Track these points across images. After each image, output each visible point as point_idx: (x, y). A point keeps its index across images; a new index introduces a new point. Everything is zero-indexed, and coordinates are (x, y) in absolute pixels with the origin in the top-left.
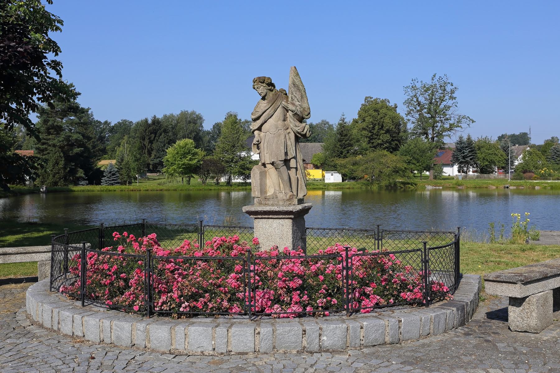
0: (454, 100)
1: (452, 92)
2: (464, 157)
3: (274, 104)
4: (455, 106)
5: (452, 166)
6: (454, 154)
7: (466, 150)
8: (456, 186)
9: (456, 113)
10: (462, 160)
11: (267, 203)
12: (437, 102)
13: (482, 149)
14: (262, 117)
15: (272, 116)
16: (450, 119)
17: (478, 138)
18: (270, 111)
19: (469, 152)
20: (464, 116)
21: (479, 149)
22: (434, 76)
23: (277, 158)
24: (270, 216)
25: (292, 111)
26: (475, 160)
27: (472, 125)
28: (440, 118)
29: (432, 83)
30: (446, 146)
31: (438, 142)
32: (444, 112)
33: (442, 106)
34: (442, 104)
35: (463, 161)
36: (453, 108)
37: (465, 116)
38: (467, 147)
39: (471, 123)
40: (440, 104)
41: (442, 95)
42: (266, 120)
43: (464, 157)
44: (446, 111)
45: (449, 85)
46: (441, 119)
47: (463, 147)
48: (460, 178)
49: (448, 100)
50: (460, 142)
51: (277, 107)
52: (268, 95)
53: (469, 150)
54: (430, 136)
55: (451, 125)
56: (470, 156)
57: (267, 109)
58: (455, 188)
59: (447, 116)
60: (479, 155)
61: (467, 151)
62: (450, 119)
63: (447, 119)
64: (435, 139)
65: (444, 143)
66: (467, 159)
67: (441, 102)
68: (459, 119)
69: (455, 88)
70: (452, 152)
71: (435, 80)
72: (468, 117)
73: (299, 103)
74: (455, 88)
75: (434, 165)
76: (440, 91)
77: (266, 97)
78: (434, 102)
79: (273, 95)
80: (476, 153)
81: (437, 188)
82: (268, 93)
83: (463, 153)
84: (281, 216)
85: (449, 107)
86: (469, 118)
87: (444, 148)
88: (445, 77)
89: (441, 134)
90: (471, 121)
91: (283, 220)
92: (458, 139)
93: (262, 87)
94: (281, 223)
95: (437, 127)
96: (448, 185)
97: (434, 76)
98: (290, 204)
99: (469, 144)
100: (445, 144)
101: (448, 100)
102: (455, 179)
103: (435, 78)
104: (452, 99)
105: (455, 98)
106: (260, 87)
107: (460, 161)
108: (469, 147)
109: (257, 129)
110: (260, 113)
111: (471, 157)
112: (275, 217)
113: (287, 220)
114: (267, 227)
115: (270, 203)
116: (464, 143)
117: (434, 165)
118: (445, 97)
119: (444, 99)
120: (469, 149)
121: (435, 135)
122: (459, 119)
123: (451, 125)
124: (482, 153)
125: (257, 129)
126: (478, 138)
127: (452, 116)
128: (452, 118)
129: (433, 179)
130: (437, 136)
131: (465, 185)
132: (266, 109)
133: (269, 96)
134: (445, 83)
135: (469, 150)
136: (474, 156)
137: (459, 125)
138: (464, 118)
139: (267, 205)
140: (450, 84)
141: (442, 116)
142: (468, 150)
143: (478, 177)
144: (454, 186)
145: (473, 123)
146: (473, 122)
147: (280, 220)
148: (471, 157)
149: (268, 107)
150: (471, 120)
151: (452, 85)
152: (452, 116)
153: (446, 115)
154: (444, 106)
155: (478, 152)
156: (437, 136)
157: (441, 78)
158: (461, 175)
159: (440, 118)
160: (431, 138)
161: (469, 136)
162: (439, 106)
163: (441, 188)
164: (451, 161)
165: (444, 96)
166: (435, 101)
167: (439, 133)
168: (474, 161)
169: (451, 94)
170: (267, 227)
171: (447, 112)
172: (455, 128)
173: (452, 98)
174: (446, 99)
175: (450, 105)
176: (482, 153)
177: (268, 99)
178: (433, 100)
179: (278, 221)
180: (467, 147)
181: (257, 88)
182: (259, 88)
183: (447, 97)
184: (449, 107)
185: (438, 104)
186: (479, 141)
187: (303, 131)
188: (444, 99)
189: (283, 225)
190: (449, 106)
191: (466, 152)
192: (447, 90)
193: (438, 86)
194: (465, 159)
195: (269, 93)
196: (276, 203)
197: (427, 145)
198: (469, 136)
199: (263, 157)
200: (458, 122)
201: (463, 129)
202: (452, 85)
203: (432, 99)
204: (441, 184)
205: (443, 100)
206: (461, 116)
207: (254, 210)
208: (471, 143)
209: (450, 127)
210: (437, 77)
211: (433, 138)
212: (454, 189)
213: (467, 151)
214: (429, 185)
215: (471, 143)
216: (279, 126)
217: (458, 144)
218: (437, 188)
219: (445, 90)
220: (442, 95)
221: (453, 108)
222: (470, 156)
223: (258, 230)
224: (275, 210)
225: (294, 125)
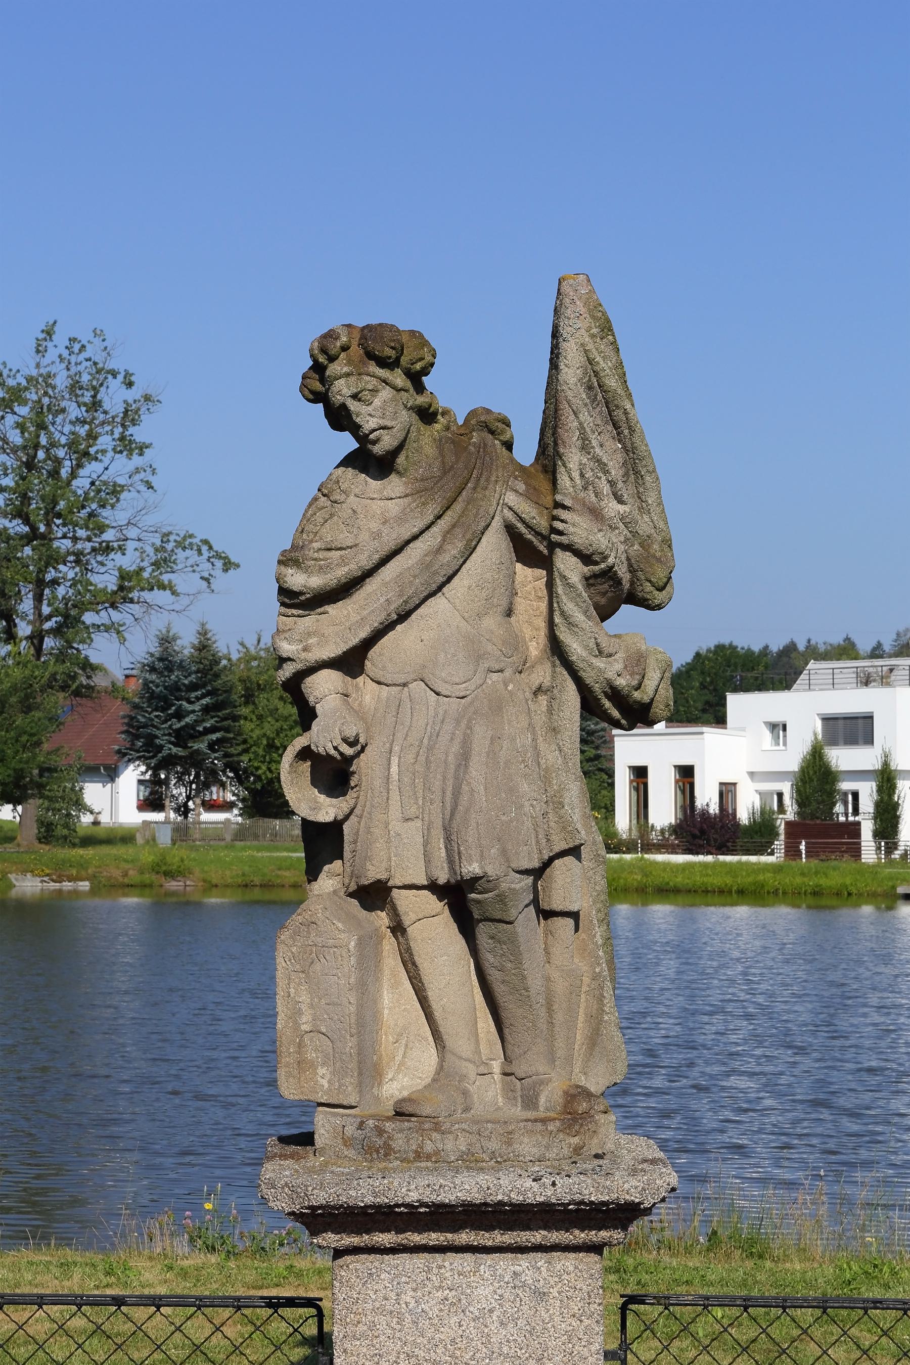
0: (135, 457)
1: (130, 416)
2: (182, 737)
3: (458, 507)
4: (143, 488)
5: (111, 774)
6: (132, 718)
7: (190, 702)
8: (154, 877)
9: (149, 520)
10: (175, 750)
11: (429, 1147)
12: (58, 462)
13: (262, 699)
14: (371, 586)
15: (449, 579)
16: (122, 549)
17: (242, 644)
18: (439, 550)
19: (206, 710)
20: (184, 538)
21: (249, 698)
22: (49, 333)
23: (504, 852)
24: (464, 1237)
25: (586, 558)
26: (232, 750)
27: (221, 580)
28: (75, 539)
29: (38, 366)
30: (99, 681)
31: (61, 657)
32: (92, 515)
33: (81, 484)
34: (82, 472)
35: (176, 756)
36: (134, 494)
37: (191, 536)
38: (193, 687)
39: (218, 572)
40: (73, 475)
41: (83, 431)
42: (410, 606)
43: (182, 737)
44: (103, 506)
45: (115, 384)
46: (79, 546)
47: (175, 688)
48: (165, 838)
49: (110, 454)
50: (161, 659)
51: (483, 524)
52: (411, 445)
53: (204, 701)
54: (24, 629)
55: (124, 576)
56: (207, 731)
57: (415, 538)
58: (151, 886)
59: (109, 535)
60: (247, 726)
61: (197, 707)
62: (122, 549)
63: (107, 549)
64: (49, 643)
65: (87, 666)
66: (196, 746)
67: (79, 466)
68: (163, 549)
69: (147, 398)
70: (125, 710)
71: (52, 355)
72: (206, 542)
73: (621, 508)
74: (147, 398)
75: (43, 770)
76: (74, 411)
77: (401, 460)
78: (45, 461)
79: (440, 443)
80: (235, 718)
81: (67, 885)
82: (413, 435)
83: (179, 715)
84: (538, 1237)
85: (116, 490)
86: (211, 548)
87: (88, 687)
88: (97, 341)
89: (78, 620)
90: (219, 564)
91: (540, 1259)
92: (154, 647)
93: (386, 393)
94: (528, 1277)
95: (55, 582)
96: (117, 873)
97: (49, 333)
98: (577, 1150)
99: (204, 672)
100: (94, 668)
101: (110, 454)
102: (140, 840)
103: (50, 344)
104: (131, 452)
105: (142, 449)
106: (375, 391)
107: (165, 752)
108: (204, 686)
109: (334, 664)
110: (365, 560)
111: (214, 737)
112: (498, 1237)
113: (568, 1262)
114: (431, 1307)
115: (449, 1146)
116: (181, 666)
117: (43, 770)
118: (96, 438)
119: (92, 450)
120: (203, 696)
121: (47, 625)
122: (163, 549)
123: (124, 576)
124: (260, 718)
125: (334, 664)
126: (242, 644)
127: (132, 533)
128: (130, 545)
129: (36, 843)
130: (57, 632)
131: (197, 870)
132: (407, 536)
133: (419, 450)
134: (99, 372)
135: (204, 701)
136: (227, 730)
137: (165, 578)
138: (184, 549)
139: (428, 1157)
140: (120, 378)
141: (82, 533)
142: (198, 699)
143: (241, 834)
144: (147, 877)
145: (226, 570)
146: (228, 565)
147: (523, 1262)
148: (214, 737)
149: (420, 524)
150: (218, 556)
151: (130, 385)
152: (132, 533)
153: (102, 529)
154: (93, 483)
155: (245, 711)
156: (57, 632)
157: (77, 347)
158: (167, 821)
159: (75, 539)
160: (30, 638)
161: (203, 633)
162: (69, 483)
163: (85, 885)
164: (119, 752)
165: (92, 436)
166: (48, 457)
167: (66, 616)
168: (226, 755)
169: (123, 425)
170: (431, 1307)
171: (105, 512)
172: (146, 595)
173: (127, 446)
174: (104, 452)
175: (121, 481)
176: (260, 718)
177: (413, 473)
178: (41, 455)
179: (505, 1264)
180: (193, 687)
181: (355, 397)
182: (366, 395)
183: (105, 441)
184: (116, 490)
185: (64, 472)
186: (248, 658)
187: (638, 688)
188: (92, 450)
189: (541, 1295)
190: (115, 485)
191: (193, 708)
192: (106, 406)
193: (61, 381)
194: (185, 747)
195: (419, 430)
196: (494, 1145)
197: (17, 674)
198: (203, 633)
199: (380, 845)
200: (156, 564)
201: (184, 601)
202: (130, 385)
203: (37, 446)
204: (82, 865)
205: (86, 454)
206: (172, 538)
207: (369, 1200)
208: (215, 669)
209: (121, 588)
210: (60, 339)
211: (37, 638)
212: (147, 891)
213: (197, 707)
214: (24, 872)
215: (215, 669)
216: (490, 647)
217: (153, 669)
218: (67, 885)
219: (95, 405)
220: (83, 431)
221: (134, 494)
222: (207, 731)
223: (362, 1328)
224: (516, 1198)
225: (592, 644)
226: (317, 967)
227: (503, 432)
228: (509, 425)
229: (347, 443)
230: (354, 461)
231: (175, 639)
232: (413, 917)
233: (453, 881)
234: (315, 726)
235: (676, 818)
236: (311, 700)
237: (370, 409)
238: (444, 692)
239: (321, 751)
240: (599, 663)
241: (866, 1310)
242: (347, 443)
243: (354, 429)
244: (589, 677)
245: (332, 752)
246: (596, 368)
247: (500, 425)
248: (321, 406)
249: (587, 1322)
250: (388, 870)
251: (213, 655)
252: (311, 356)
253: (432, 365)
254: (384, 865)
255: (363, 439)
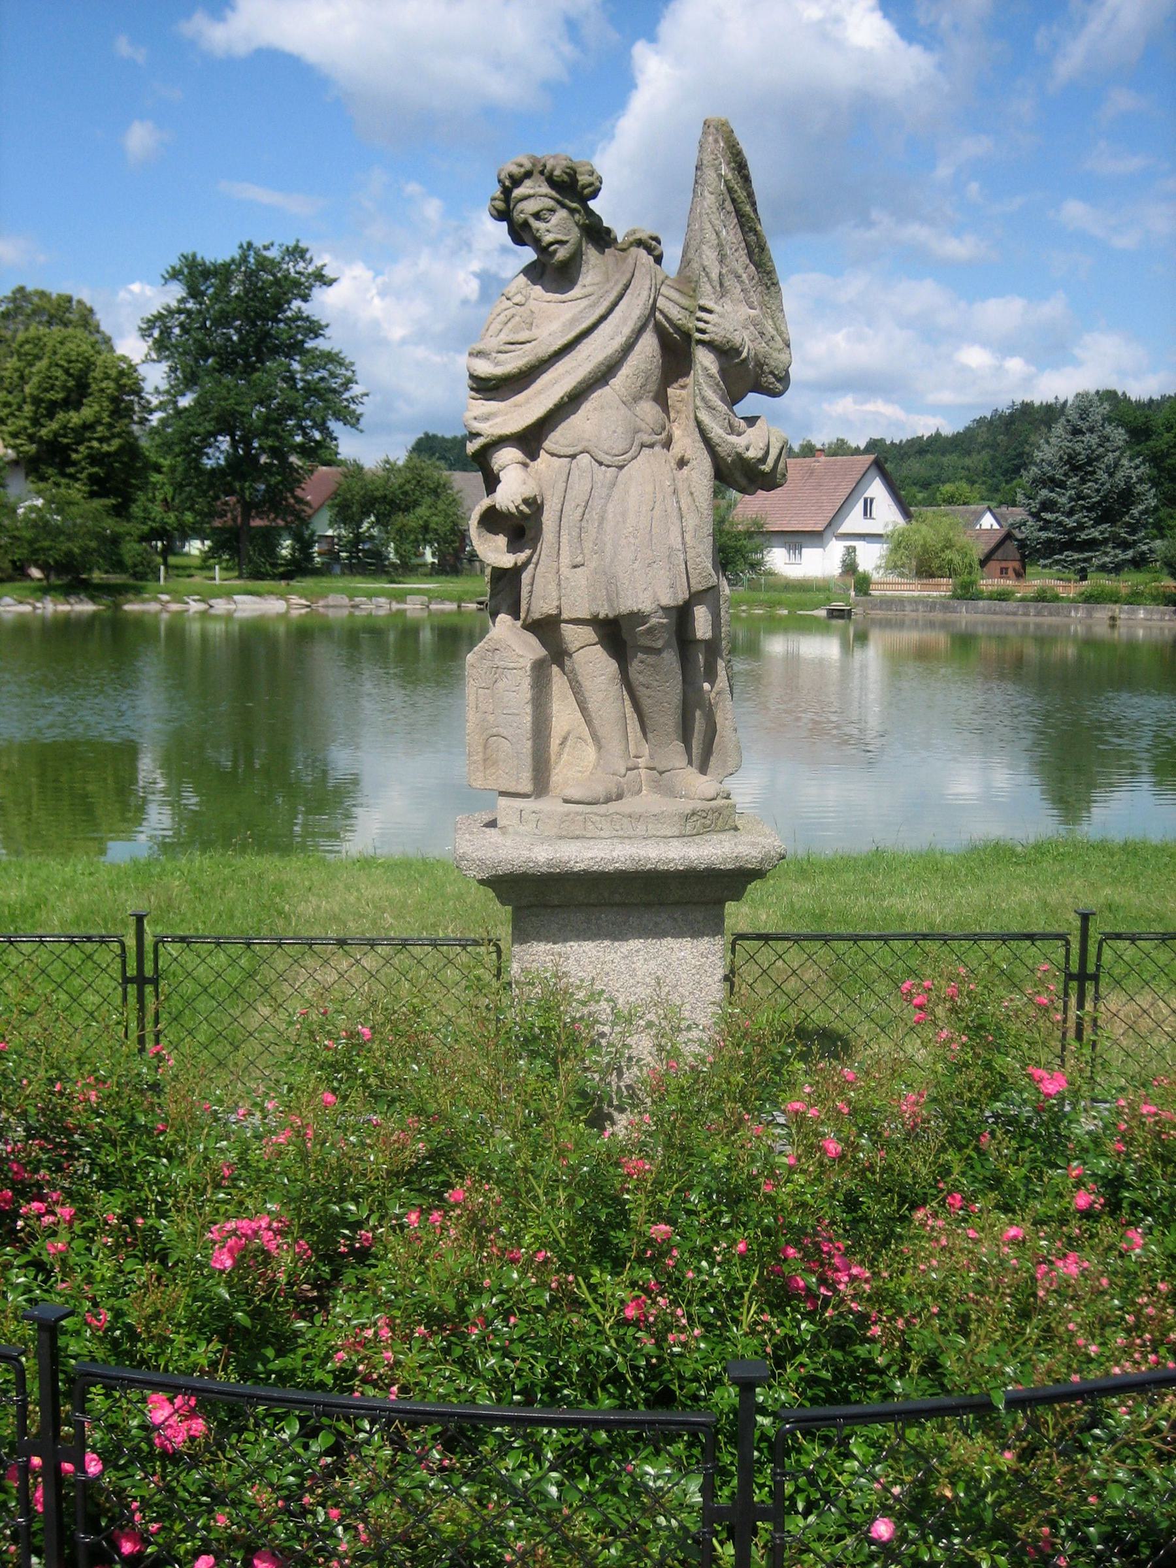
93: (562, 213)
149: (612, 297)
182: (546, 215)
225: (726, 424)
226: (500, 684)
227: (655, 248)
228: (659, 243)
229: (528, 255)
230: (535, 273)
231: (173, 268)
232: (578, 645)
233: (611, 616)
234: (500, 488)
235: (476, 471)
236: (496, 468)
237: (548, 225)
238: (606, 462)
239: (504, 509)
240: (733, 439)
241: (916, 941)
242: (528, 255)
243: (536, 243)
244: (722, 451)
245: (514, 510)
246: (735, 196)
247: (654, 243)
248: (505, 225)
249: (712, 958)
250: (559, 607)
251: (921, 856)
252: (499, 181)
253: (599, 189)
254: (556, 603)
255: (543, 250)
